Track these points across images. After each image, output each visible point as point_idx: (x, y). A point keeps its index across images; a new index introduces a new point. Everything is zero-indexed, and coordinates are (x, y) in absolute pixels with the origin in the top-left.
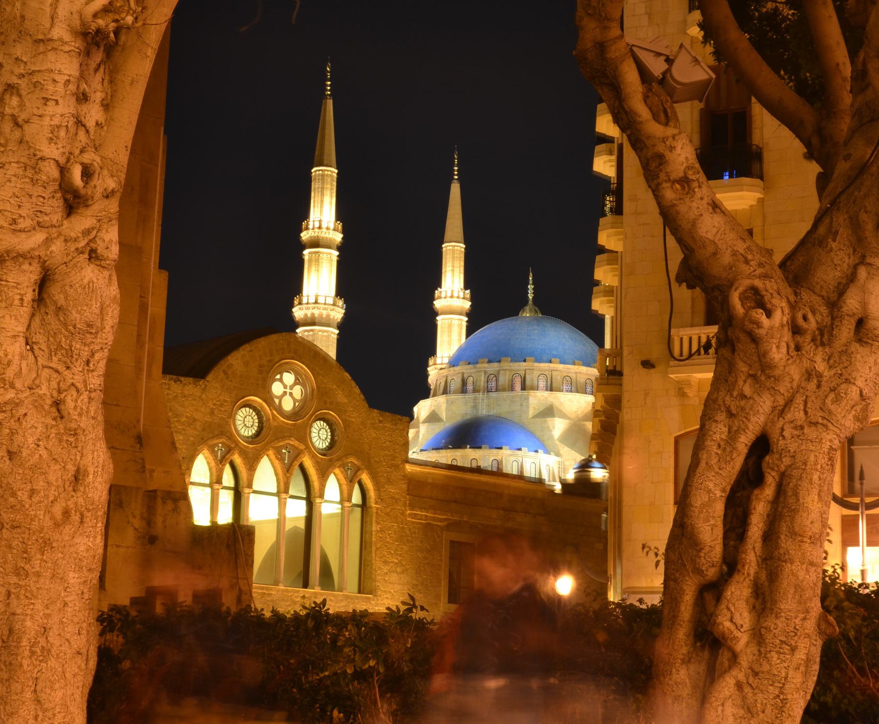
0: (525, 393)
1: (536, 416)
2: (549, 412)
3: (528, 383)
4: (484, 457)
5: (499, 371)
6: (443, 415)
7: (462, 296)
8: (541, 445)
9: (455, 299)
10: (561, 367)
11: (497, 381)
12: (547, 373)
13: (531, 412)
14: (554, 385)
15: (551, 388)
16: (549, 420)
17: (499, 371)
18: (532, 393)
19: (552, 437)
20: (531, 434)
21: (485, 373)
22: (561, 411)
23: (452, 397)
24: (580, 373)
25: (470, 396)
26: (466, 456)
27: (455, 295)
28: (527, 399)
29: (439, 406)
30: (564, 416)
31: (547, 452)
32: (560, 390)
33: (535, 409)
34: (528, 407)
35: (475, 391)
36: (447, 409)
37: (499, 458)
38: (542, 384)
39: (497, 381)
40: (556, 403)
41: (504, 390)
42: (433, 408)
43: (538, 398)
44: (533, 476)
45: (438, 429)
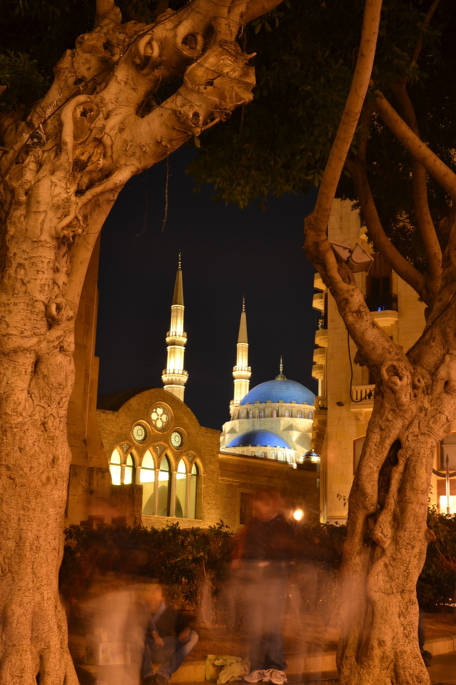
0: (278, 418)
1: (283, 431)
2: (290, 428)
3: (280, 413)
4: (258, 451)
5: (265, 408)
6: (238, 430)
8: (287, 444)
11: (264, 412)
12: (289, 408)
13: (282, 428)
15: (291, 416)
17: (265, 408)
18: (282, 418)
20: (282, 439)
21: (259, 408)
22: (296, 427)
23: (242, 420)
25: (251, 420)
26: (249, 450)
27: (244, 369)
28: (279, 421)
30: (298, 430)
31: (289, 448)
33: (283, 426)
34: (280, 425)
35: (253, 417)
36: (239, 427)
37: (265, 451)
38: (287, 414)
40: (294, 424)
41: (268, 417)
42: (232, 426)
43: (285, 421)
44: (282, 460)
45: (235, 436)
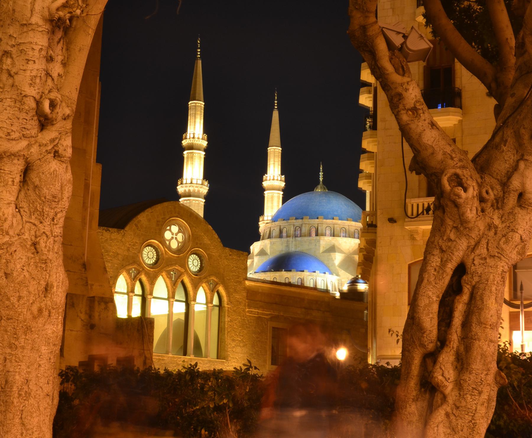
0: (318, 238)
1: (324, 252)
2: (332, 249)
3: (319, 231)
4: (293, 277)
5: (302, 225)
6: (268, 251)
7: (279, 179)
8: (328, 269)
9: (275, 181)
10: (340, 222)
11: (301, 230)
12: (331, 226)
13: (322, 249)
14: (335, 233)
15: (333, 235)
16: (332, 254)
17: (302, 225)
18: (322, 238)
19: (334, 264)
20: (322, 263)
21: (294, 225)
22: (339, 249)
23: (274, 240)
24: (351, 226)
25: (284, 240)
26: (282, 276)
27: (276, 178)
28: (319, 241)
29: (266, 246)
30: (341, 252)
31: (331, 273)
32: (339, 236)
33: (324, 247)
34: (319, 246)
35: (288, 236)
36: (271, 248)
37: (302, 277)
38: (328, 232)
39: (301, 230)
40: (336, 244)
41: (305, 236)
42: (262, 247)
43: (326, 241)
44: (323, 288)
45: (265, 259)
